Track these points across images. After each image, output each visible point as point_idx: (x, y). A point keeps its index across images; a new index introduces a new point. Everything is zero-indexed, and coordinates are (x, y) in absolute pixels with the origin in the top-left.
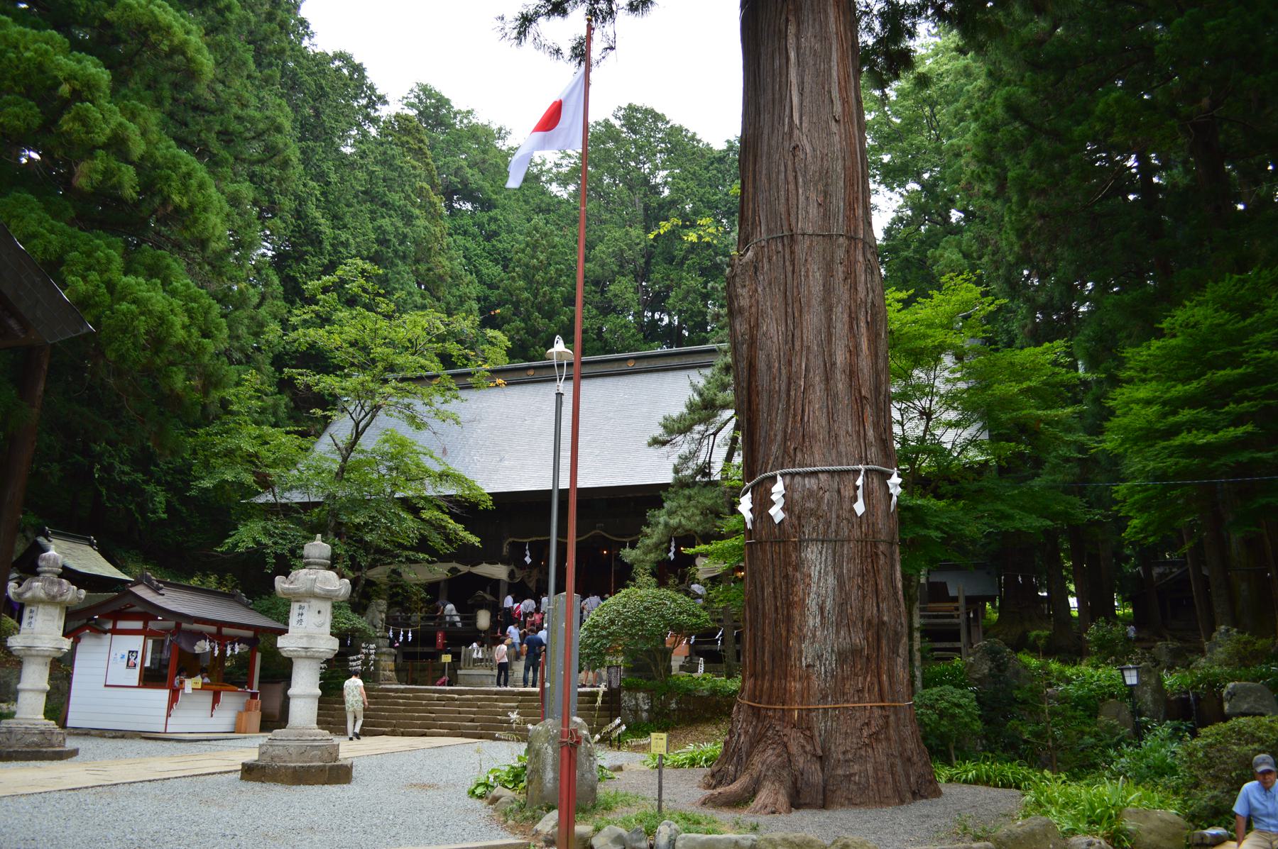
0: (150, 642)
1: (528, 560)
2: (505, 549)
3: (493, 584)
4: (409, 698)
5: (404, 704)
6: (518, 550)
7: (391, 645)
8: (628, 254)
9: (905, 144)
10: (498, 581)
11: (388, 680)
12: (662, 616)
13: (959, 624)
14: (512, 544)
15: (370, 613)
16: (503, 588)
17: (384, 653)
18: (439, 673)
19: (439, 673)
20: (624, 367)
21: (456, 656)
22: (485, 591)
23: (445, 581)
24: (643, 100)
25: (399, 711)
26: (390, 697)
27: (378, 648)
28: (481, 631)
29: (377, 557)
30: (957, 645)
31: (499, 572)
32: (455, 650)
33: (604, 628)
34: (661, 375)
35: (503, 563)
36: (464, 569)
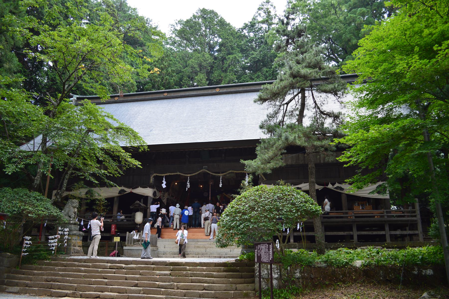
0: (50, 237)
1: (164, 186)
2: (152, 180)
3: (145, 198)
4: (89, 267)
5: (85, 271)
6: (159, 180)
7: (80, 230)
8: (204, 64)
9: (327, 19)
10: (147, 197)
11: (77, 253)
12: (293, 204)
13: (416, 221)
14: (155, 177)
15: (67, 209)
16: (150, 201)
17: (75, 235)
18: (112, 248)
19: (112, 248)
20: (214, 91)
21: (123, 239)
22: (140, 201)
23: (117, 197)
24: (209, 7)
25: (80, 276)
26: (75, 266)
27: (70, 231)
28: (137, 224)
29: (74, 172)
30: (416, 232)
31: (148, 192)
32: (123, 235)
33: (244, 214)
34: (234, 95)
35: (150, 187)
36: (128, 190)
